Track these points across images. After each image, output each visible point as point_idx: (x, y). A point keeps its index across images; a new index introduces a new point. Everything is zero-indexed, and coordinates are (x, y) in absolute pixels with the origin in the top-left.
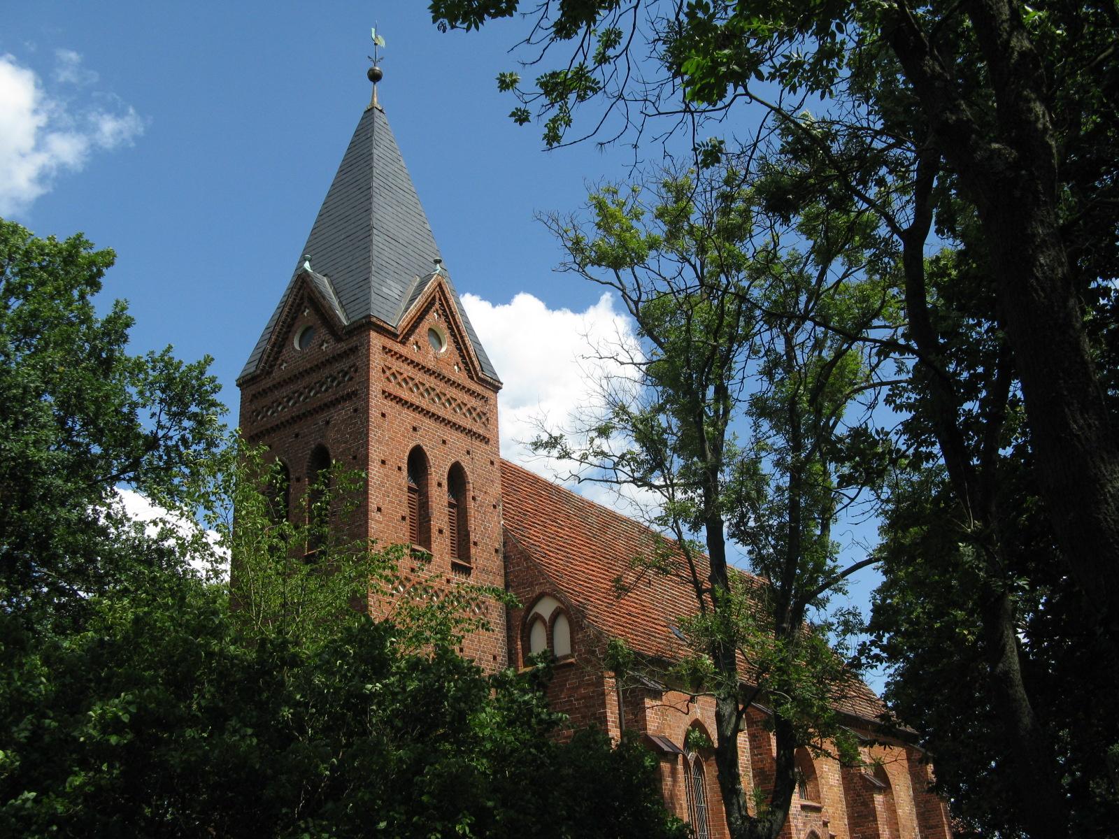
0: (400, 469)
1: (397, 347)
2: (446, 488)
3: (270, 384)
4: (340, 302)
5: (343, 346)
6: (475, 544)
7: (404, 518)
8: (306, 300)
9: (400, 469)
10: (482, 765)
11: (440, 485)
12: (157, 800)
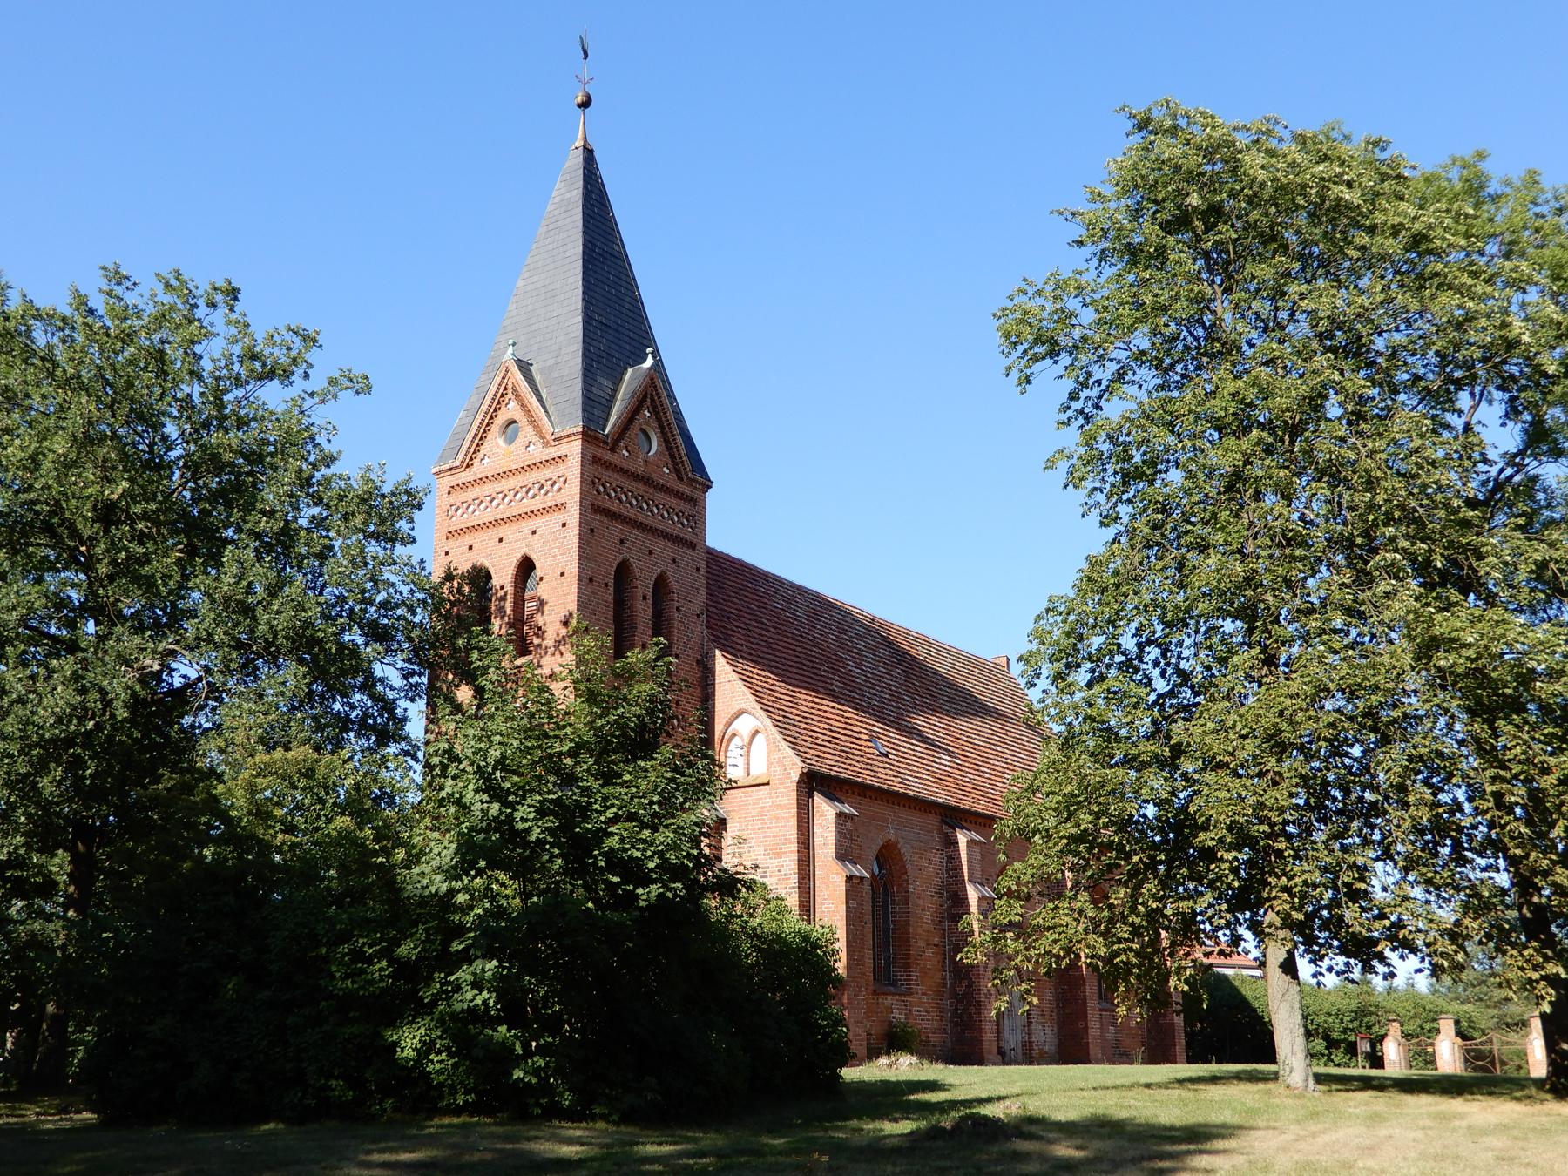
0: (606, 585)
1: (609, 456)
2: (650, 601)
3: (471, 479)
4: (928, 1053)
5: (553, 452)
8: (510, 391)
9: (606, 585)
10: (1151, 811)
11: (645, 598)
12: (1541, 896)
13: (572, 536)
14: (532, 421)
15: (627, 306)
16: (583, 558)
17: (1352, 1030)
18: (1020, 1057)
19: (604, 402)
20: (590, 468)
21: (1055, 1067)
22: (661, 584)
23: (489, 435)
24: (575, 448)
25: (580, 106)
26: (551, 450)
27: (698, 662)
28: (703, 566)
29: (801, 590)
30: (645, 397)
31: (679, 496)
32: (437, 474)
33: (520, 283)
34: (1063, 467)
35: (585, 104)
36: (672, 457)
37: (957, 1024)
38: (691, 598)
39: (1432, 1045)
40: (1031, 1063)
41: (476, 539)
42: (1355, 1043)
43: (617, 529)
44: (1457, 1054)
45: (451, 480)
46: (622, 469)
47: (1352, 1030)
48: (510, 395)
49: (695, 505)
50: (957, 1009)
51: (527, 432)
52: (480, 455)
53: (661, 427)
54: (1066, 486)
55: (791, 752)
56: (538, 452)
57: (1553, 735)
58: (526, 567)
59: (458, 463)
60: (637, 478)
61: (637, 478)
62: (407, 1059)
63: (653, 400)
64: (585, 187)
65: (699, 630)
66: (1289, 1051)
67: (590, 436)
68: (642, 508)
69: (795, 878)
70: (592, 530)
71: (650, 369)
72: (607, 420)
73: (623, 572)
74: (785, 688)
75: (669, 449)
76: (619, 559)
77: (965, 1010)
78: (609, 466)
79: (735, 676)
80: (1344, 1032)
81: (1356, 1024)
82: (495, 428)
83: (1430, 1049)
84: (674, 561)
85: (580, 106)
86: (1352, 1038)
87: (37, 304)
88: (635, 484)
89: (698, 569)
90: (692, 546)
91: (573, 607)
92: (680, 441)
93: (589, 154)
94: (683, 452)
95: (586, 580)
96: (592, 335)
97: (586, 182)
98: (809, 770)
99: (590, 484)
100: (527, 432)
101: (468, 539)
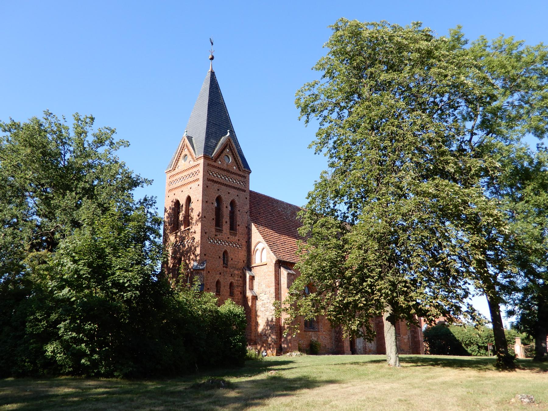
1: (213, 164)
5: (196, 163)
6: (239, 225)
7: (213, 219)
13: (201, 188)
14: (191, 154)
15: (224, 118)
16: (204, 195)
17: (486, 342)
18: (362, 351)
19: (213, 147)
20: (207, 167)
21: (373, 355)
22: (233, 203)
23: (180, 159)
24: (201, 161)
25: (210, 59)
26: (196, 162)
27: (246, 227)
28: (248, 197)
29: (290, 205)
30: (227, 145)
31: (239, 175)
32: (166, 173)
33: (192, 114)
34: (314, 147)
35: (212, 59)
36: (237, 163)
37: (336, 341)
38: (243, 206)
39: (514, 347)
40: (365, 354)
41: (175, 192)
42: (487, 346)
43: (216, 186)
44: (522, 350)
45: (170, 174)
46: (218, 167)
47: (486, 342)
48: (185, 147)
49: (245, 178)
50: (336, 336)
51: (189, 158)
52: (177, 166)
53: (233, 154)
54: (315, 153)
55: (273, 254)
56: (193, 163)
57: (470, 228)
58: (189, 199)
59: (171, 169)
60: (224, 170)
61: (224, 170)
62: (49, 356)
63: (230, 146)
64: (211, 83)
65: (247, 217)
66: (390, 351)
67: (206, 157)
68: (226, 179)
69: (274, 294)
70: (207, 186)
71: (228, 136)
72: (213, 152)
73: (219, 200)
74: (277, 235)
75: (236, 161)
76: (217, 195)
77: (339, 336)
78: (214, 166)
79: (257, 231)
80: (483, 343)
81: (487, 340)
82: (181, 157)
83: (513, 348)
84: (238, 196)
85: (210, 59)
86: (486, 345)
87: (15, 121)
88: (223, 172)
89: (246, 198)
90: (245, 191)
91: (200, 211)
92: (239, 158)
93: (213, 74)
94: (241, 162)
95: (205, 202)
96: (210, 127)
97: (211, 82)
98: (278, 260)
99: (206, 172)
100: (189, 158)
101: (174, 192)
